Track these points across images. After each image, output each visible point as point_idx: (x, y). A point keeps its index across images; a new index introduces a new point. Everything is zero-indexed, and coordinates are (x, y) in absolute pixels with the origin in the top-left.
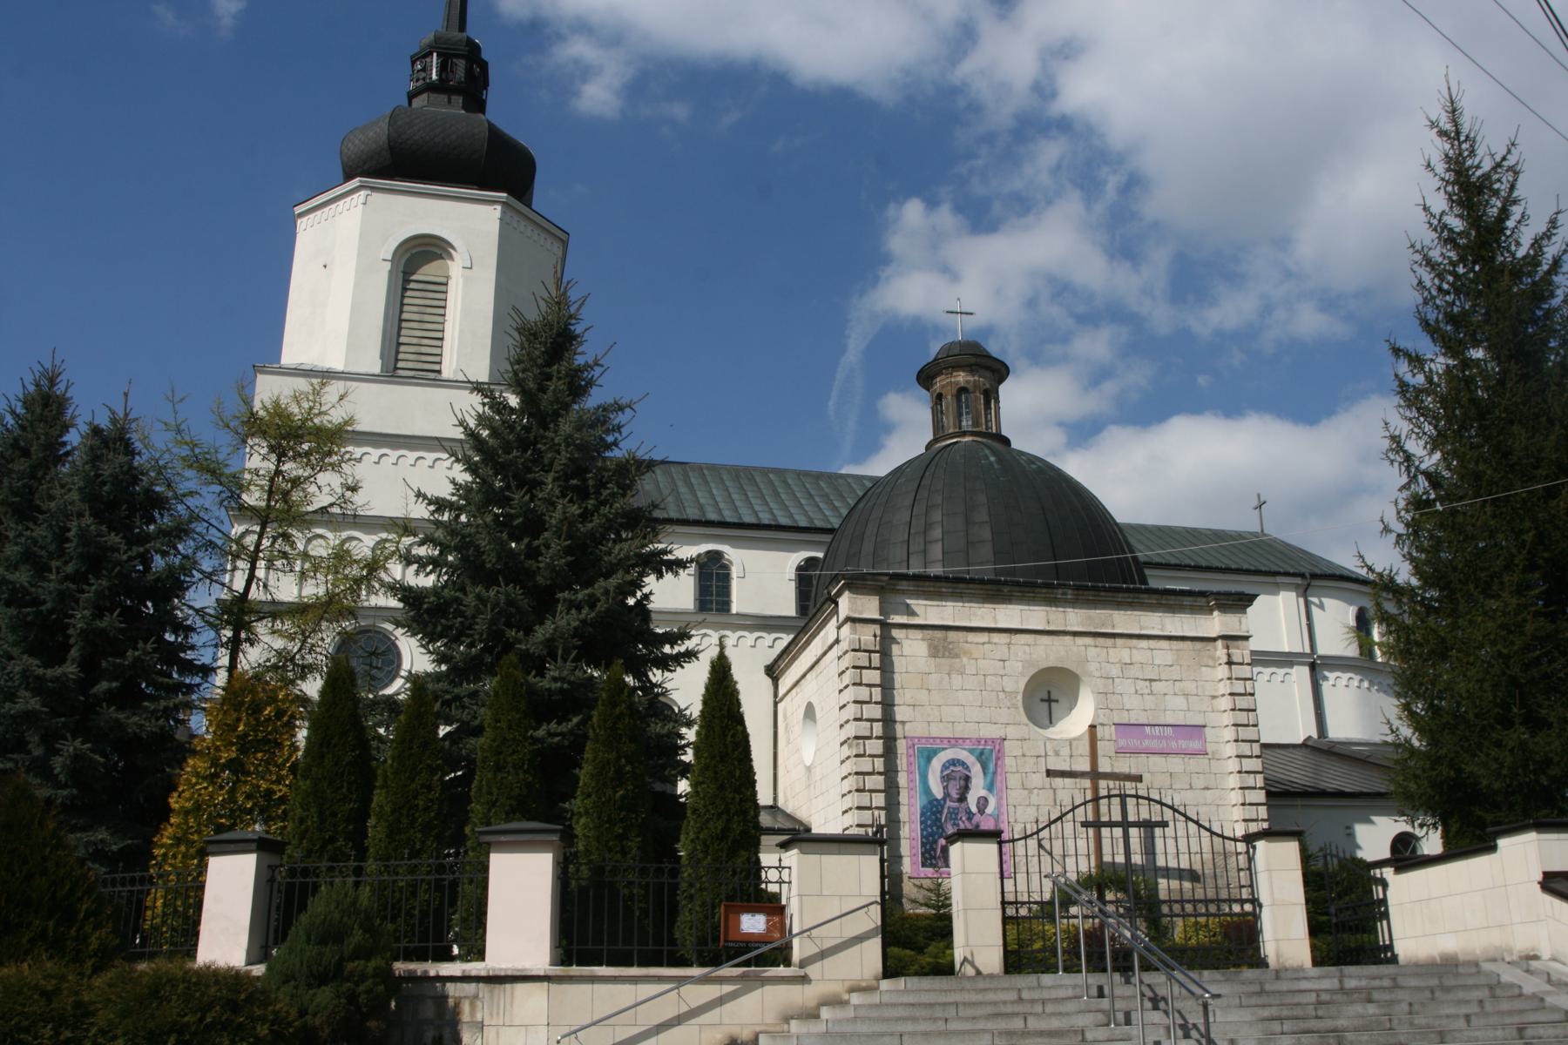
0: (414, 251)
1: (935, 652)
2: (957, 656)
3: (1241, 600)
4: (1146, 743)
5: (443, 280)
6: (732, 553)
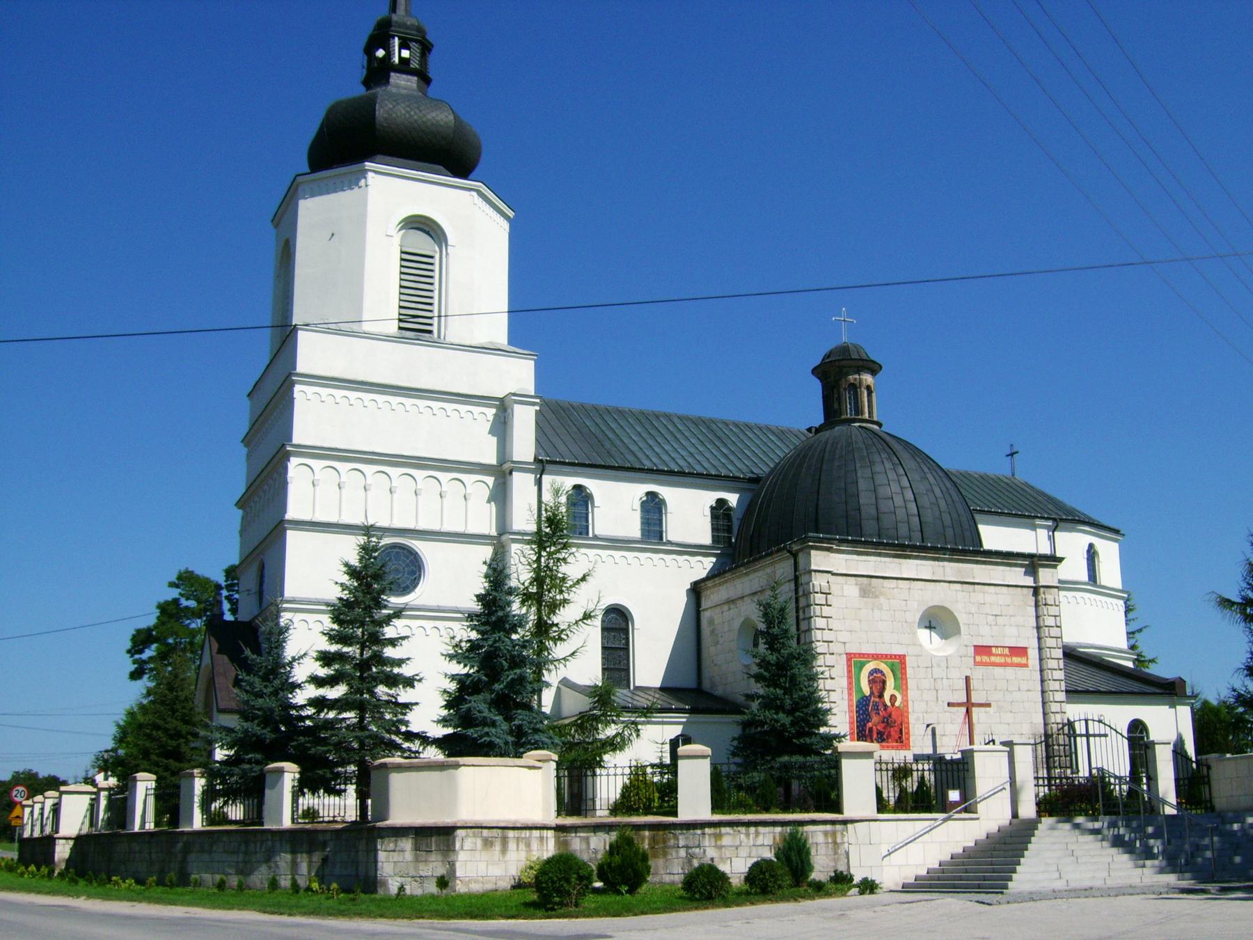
1: (864, 593)
2: (876, 597)
3: (1054, 561)
4: (993, 659)
6: (665, 492)
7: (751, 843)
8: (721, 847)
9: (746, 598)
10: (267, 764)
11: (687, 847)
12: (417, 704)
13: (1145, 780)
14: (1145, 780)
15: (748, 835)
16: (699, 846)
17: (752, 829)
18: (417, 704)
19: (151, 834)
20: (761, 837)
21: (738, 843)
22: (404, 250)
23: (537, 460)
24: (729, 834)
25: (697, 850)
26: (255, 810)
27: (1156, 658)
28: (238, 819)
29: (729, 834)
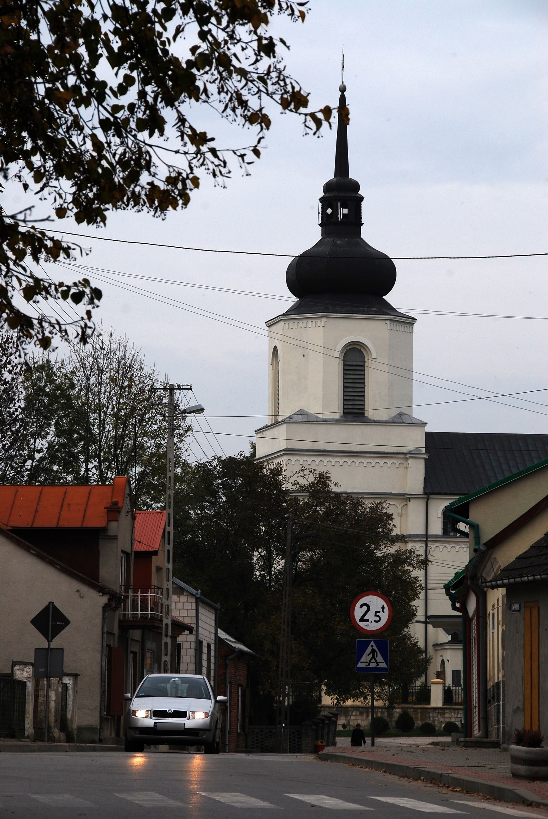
0: (347, 349)
5: (361, 364)
7: (456, 716)
8: (445, 717)
9: (302, 115)
10: (160, 56)
11: (433, 717)
12: (71, 187)
13: (162, 685)
14: (162, 685)
15: (455, 713)
16: (437, 717)
17: (456, 711)
18: (71, 187)
19: (463, 646)
20: (459, 715)
21: (451, 716)
22: (346, 363)
23: (425, 493)
24: (448, 713)
25: (436, 718)
26: (212, 653)
27: (79, 675)
28: (462, 647)
29: (448, 713)
